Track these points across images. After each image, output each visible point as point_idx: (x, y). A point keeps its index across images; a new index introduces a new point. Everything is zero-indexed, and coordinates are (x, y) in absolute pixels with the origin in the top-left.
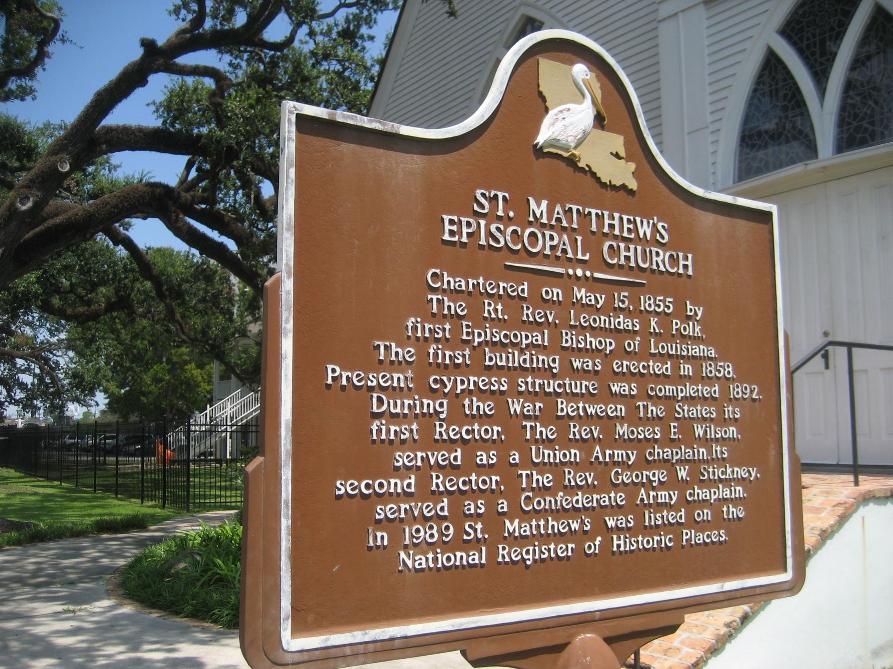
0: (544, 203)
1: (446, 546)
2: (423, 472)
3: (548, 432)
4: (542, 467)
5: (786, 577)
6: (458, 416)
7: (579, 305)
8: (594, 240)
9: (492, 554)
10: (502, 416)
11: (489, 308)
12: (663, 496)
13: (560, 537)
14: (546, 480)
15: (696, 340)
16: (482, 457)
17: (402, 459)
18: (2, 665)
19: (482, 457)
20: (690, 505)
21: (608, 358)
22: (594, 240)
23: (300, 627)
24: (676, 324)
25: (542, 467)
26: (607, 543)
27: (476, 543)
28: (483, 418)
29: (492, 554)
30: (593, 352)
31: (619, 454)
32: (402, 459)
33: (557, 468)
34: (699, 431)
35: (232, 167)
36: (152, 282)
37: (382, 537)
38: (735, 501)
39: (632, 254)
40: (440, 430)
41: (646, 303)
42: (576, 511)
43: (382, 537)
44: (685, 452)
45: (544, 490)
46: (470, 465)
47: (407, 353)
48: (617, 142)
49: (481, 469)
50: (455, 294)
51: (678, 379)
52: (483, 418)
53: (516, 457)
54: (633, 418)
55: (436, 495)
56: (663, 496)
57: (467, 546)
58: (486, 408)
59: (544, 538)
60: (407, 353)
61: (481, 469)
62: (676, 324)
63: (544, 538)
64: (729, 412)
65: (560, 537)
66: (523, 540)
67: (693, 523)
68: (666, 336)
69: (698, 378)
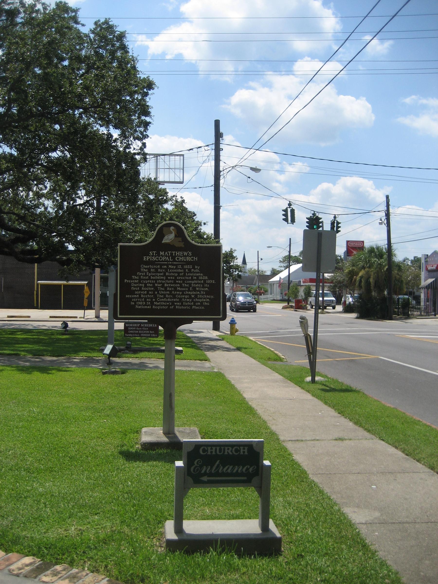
0: (163, 252)
1: (144, 305)
2: (140, 295)
3: (163, 289)
4: (162, 294)
5: (221, 317)
6: (146, 286)
7: (170, 269)
8: (173, 258)
9: (152, 307)
10: (154, 286)
11: (152, 270)
12: (188, 300)
13: (164, 305)
14: (162, 296)
15: (198, 273)
16: (150, 293)
17: (136, 293)
18: (1, 254)
19: (150, 293)
20: (195, 303)
21: (176, 277)
22: (173, 258)
23: (120, 315)
24: (192, 270)
25: (162, 294)
26: (175, 307)
27: (149, 305)
28: (150, 287)
29: (152, 307)
30: (173, 276)
31: (178, 293)
32: (136, 293)
33: (165, 295)
34: (197, 289)
35: (35, 241)
36: (36, 250)
37: (133, 303)
38: (207, 302)
39: (182, 259)
40: (143, 289)
41: (186, 267)
42: (168, 302)
43: (133, 303)
44: (193, 293)
45: (162, 298)
46: (148, 294)
47: (138, 278)
48: (180, 239)
49: (150, 294)
50: (145, 269)
51: (192, 280)
52: (150, 287)
53: (156, 293)
54: (181, 287)
55: (142, 298)
56: (188, 300)
57: (147, 306)
58: (151, 285)
59: (162, 305)
60: (138, 278)
61: (150, 294)
62: (192, 270)
63: (162, 305)
64: (206, 285)
65: (164, 305)
66: (158, 305)
67: (194, 305)
68: (190, 272)
69: (198, 279)
